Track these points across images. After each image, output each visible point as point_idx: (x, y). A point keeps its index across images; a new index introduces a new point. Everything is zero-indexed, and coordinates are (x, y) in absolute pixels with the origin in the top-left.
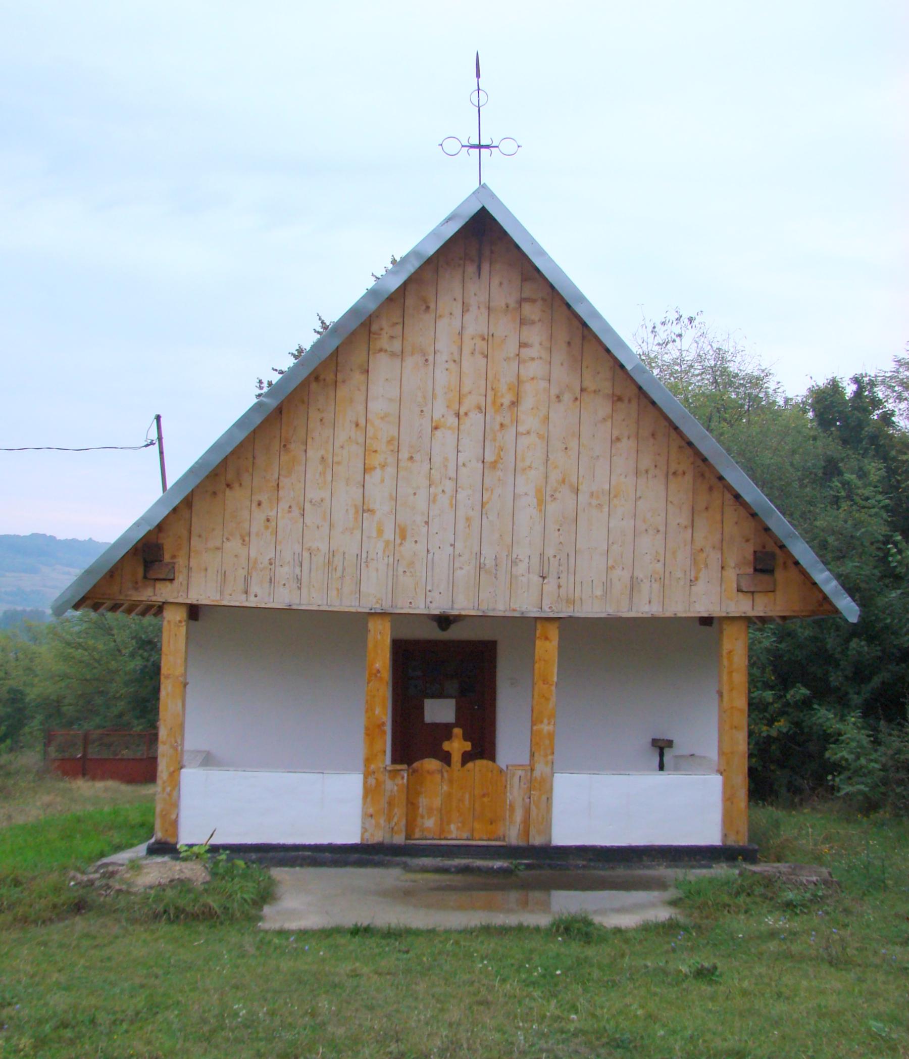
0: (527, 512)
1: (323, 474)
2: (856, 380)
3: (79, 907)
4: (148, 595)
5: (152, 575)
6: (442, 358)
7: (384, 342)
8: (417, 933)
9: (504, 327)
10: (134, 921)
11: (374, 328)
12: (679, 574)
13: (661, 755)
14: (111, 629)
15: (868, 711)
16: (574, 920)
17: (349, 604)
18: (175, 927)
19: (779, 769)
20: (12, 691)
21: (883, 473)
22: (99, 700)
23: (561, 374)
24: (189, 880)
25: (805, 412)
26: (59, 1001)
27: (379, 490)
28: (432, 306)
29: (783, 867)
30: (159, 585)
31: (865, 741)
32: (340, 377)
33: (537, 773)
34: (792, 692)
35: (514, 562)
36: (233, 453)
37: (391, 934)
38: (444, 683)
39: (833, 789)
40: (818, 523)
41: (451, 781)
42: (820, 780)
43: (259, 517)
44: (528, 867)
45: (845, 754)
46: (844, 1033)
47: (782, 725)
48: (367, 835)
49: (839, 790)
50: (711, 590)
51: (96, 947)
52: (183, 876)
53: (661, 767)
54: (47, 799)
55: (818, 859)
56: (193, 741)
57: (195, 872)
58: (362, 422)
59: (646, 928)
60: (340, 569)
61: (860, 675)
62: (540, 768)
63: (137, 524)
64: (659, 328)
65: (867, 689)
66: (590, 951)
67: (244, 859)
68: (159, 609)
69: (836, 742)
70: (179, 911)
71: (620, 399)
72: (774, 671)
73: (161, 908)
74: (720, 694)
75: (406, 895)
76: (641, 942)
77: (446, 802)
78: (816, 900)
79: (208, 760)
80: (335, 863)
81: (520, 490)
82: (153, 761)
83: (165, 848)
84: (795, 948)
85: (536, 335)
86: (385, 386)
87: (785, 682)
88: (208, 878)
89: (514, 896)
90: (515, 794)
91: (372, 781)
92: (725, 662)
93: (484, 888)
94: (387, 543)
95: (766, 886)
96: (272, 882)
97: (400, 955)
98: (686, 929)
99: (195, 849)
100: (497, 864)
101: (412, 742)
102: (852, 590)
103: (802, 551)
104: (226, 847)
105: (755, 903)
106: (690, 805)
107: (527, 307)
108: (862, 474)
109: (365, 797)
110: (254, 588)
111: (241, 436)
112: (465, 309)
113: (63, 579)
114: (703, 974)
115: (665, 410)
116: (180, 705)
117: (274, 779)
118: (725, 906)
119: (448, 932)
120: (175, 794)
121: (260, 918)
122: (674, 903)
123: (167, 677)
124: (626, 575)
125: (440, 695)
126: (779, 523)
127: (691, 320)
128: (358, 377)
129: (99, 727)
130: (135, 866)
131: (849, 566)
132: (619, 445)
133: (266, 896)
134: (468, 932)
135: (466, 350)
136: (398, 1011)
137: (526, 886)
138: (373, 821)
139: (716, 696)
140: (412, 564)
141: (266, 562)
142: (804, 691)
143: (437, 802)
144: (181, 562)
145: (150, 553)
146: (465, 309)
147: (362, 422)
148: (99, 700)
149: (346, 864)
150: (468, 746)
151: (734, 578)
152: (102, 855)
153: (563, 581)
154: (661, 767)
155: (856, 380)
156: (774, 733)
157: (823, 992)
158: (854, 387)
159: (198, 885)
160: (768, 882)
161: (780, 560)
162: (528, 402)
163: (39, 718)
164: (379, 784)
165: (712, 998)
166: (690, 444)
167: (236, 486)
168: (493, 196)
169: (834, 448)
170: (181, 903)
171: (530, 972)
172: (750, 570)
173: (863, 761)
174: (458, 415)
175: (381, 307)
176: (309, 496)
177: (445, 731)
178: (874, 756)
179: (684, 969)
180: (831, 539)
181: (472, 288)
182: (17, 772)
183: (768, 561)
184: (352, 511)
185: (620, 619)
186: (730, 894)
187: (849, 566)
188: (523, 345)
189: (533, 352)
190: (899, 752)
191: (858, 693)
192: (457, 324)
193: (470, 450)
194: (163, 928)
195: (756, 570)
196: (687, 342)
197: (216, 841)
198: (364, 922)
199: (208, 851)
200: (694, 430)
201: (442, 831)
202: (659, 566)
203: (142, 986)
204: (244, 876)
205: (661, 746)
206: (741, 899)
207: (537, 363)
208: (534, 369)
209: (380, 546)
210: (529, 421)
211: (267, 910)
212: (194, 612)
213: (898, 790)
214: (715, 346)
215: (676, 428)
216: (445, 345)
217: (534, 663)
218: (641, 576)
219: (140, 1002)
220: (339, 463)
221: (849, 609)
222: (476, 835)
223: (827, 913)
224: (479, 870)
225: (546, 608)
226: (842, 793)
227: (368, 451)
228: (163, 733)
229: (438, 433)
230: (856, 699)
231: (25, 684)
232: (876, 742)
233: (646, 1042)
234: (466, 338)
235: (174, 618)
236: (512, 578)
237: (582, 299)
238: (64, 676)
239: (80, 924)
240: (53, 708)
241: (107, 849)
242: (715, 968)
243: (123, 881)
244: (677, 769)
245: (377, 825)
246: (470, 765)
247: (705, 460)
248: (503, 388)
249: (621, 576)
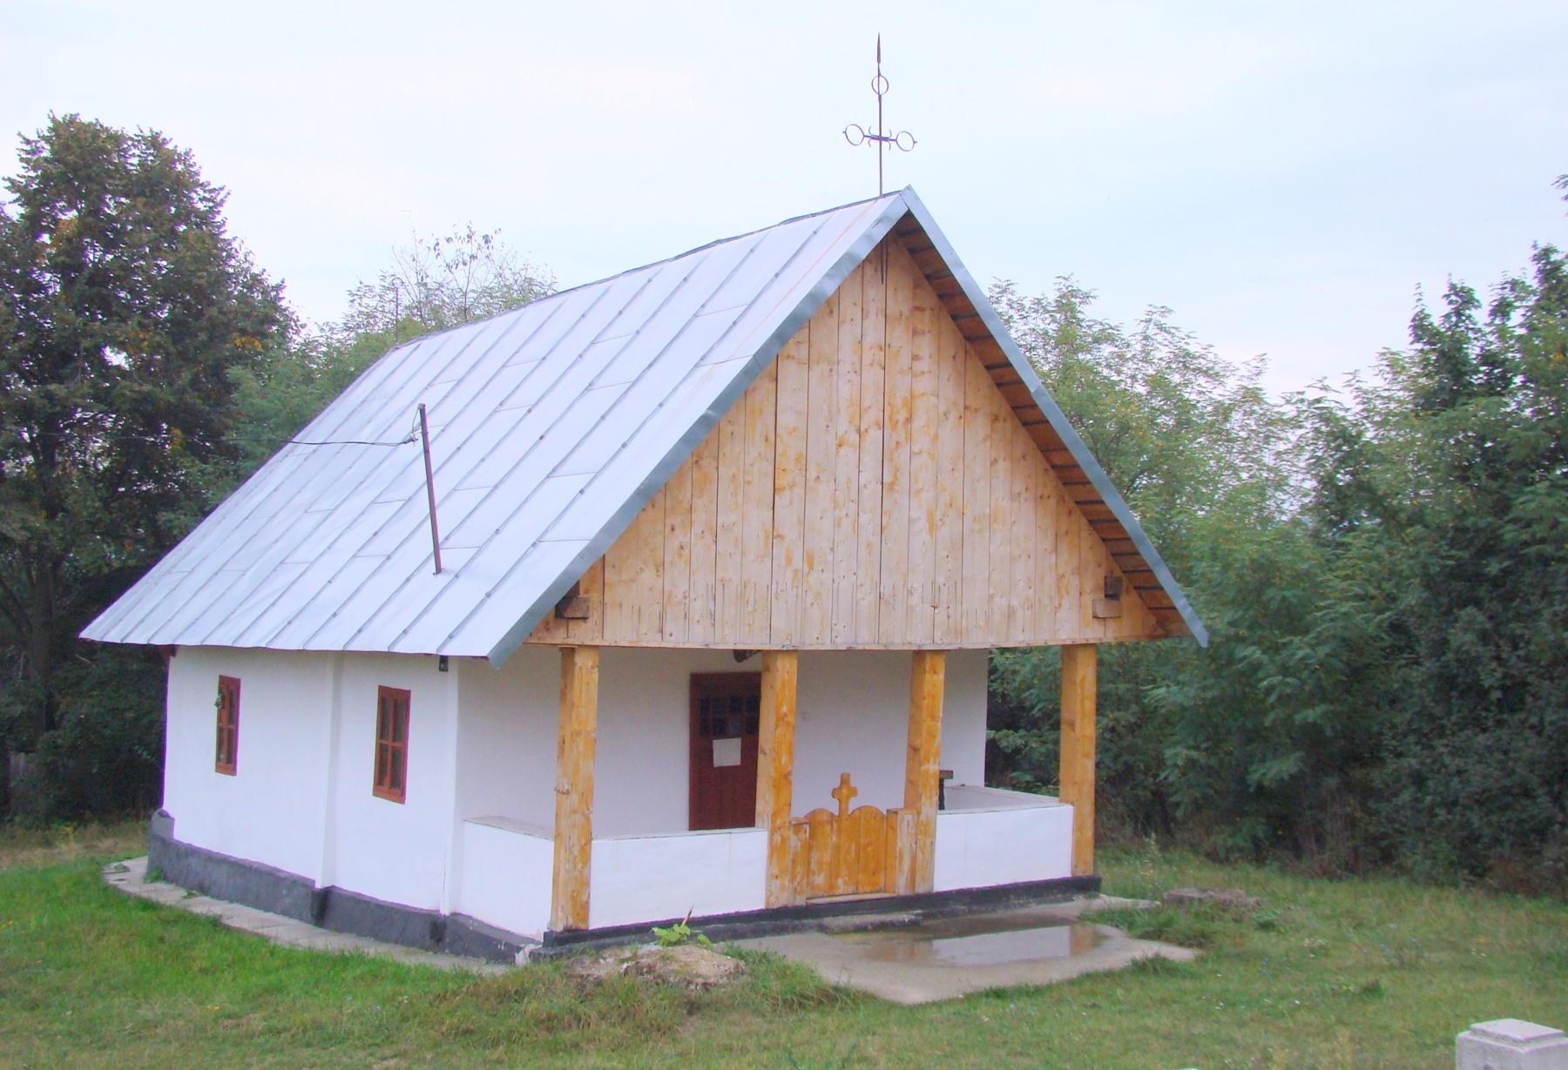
6: (845, 367)
9: (899, 337)
30: (572, 624)
35: (910, 593)
48: (772, 899)
91: (777, 838)
100: (905, 917)
109: (771, 856)
112: (864, 314)
135: (866, 361)
140: (819, 594)
141: (680, 595)
143: (827, 857)
146: (864, 314)
151: (1090, 604)
162: (918, 423)
164: (784, 840)
188: (915, 358)
208: (924, 384)
209: (789, 574)
210: (921, 442)
216: (847, 356)
220: (749, 483)
225: (937, 640)
229: (842, 451)
234: (866, 346)
236: (909, 610)
245: (782, 886)
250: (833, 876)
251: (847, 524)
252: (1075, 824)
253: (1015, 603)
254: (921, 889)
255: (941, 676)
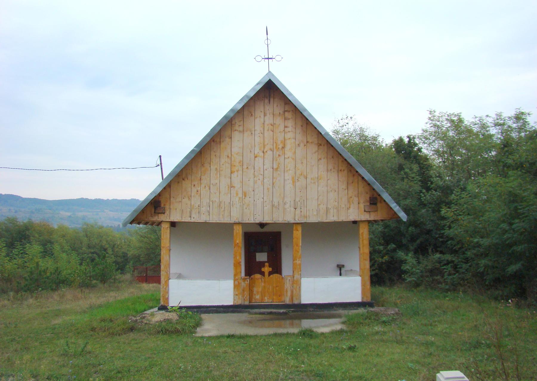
0: (289, 185)
1: (216, 174)
2: (408, 137)
3: (132, 329)
4: (156, 219)
5: (157, 211)
7: (237, 127)
8: (250, 336)
9: (279, 121)
10: (150, 334)
11: (233, 123)
12: (343, 206)
13: (340, 270)
14: (156, 231)
15: (416, 252)
16: (307, 330)
17: (227, 220)
18: (165, 336)
19: (383, 274)
20: (123, 253)
21: (418, 168)
22: (152, 256)
23: (300, 136)
24: (171, 319)
25: (391, 148)
26: (118, 364)
27: (236, 179)
28: (253, 114)
29: (382, 308)
30: (159, 215)
31: (415, 262)
32: (221, 140)
33: (295, 278)
34: (390, 246)
35: (285, 204)
36: (184, 168)
37: (241, 337)
38: (263, 248)
39: (404, 280)
40: (396, 187)
41: (265, 282)
42: (400, 276)
43: (194, 190)
44: (293, 311)
45: (408, 267)
46: (400, 368)
47: (386, 258)
48: (235, 302)
49: (406, 280)
50: (355, 212)
51: (137, 343)
52: (169, 318)
53: (340, 275)
54: (132, 290)
55: (396, 305)
56: (173, 270)
57: (173, 316)
58: (230, 156)
59: (333, 332)
60: (223, 208)
61: (413, 239)
62: (296, 276)
63: (151, 194)
64: (340, 121)
65: (415, 245)
66: (312, 342)
67: (192, 311)
68: (159, 224)
69: (405, 263)
70: (167, 330)
71: (321, 145)
72: (383, 239)
73: (160, 329)
74: (359, 248)
75: (250, 323)
76: (330, 337)
77: (264, 289)
78: (394, 320)
79: (180, 276)
80: (225, 312)
81: (286, 178)
82: (159, 277)
83: (164, 308)
84: (385, 338)
85: (290, 123)
86: (237, 143)
87: (387, 243)
88: (178, 318)
89: (288, 322)
90: (288, 285)
91: (236, 283)
92: (361, 237)
93: (278, 319)
94: (240, 198)
95: (376, 316)
96: (201, 319)
97: (244, 345)
98: (346, 332)
99: (174, 308)
101: (252, 268)
102: (406, 210)
103: (386, 196)
104: (185, 307)
105: (372, 322)
106: (349, 287)
107: (286, 114)
108: (411, 169)
109: (234, 288)
110: (193, 215)
111: (187, 162)
112: (265, 115)
113: (126, 214)
114: (351, 348)
115: (336, 148)
116: (168, 256)
117: (200, 284)
118: (361, 323)
119: (261, 336)
120: (167, 288)
121: (195, 333)
122: (343, 323)
123: (163, 247)
124: (325, 207)
125: (262, 251)
126: (377, 186)
127: (351, 118)
128: (228, 140)
129: (153, 265)
130: (152, 315)
131: (408, 202)
132: (320, 161)
133: (198, 324)
134: (268, 336)
135: (266, 129)
136: (239, 365)
137: (291, 318)
138: (237, 297)
139: (358, 249)
141: (197, 206)
142: (394, 246)
143: (260, 290)
144: (167, 207)
145: (156, 204)
146: (265, 115)
147: (230, 156)
148: (152, 256)
149: (228, 312)
150: (271, 269)
152: (145, 310)
153: (302, 210)
154: (340, 275)
155: (408, 137)
156: (384, 261)
157: (393, 353)
158: (408, 139)
159: (174, 321)
160: (377, 314)
161: (379, 200)
162: (288, 147)
163: (132, 262)
165: (354, 357)
166: (346, 160)
167: (186, 179)
168: (273, 75)
169: (402, 161)
170: (167, 327)
171: (289, 350)
172: (369, 204)
173: (414, 269)
174: (264, 152)
175: (235, 114)
176: (212, 182)
177: (262, 264)
178: (418, 267)
179: (344, 347)
180: (401, 192)
181: (267, 107)
182: (123, 281)
183: (374, 201)
184: (227, 187)
185: (323, 222)
186: (363, 319)
187: (408, 202)
188: (286, 127)
189: (290, 129)
190: (427, 266)
191: (412, 246)
192: (262, 120)
193: (268, 165)
194: (160, 336)
195: (370, 204)
196: (350, 126)
197: (181, 305)
198: (232, 333)
199: (178, 309)
200: (347, 155)
201: (262, 299)
202: (336, 203)
203: (149, 358)
204: (191, 317)
205: (340, 267)
206: (367, 321)
207: (291, 134)
208: (290, 135)
209: (237, 199)
210: (289, 154)
211: (198, 329)
212: (173, 224)
213: (427, 279)
214: (360, 127)
215: (341, 155)
216: (258, 128)
217: (293, 239)
218: (330, 207)
219: (147, 364)
221: (403, 216)
222: (274, 301)
223: (397, 325)
224: (275, 313)
226: (407, 281)
227: (232, 166)
228: (162, 267)
229: (257, 159)
230: (412, 248)
231: (128, 251)
232: (419, 263)
233: (328, 374)
234: (266, 126)
235: (165, 227)
237: (305, 110)
238: (141, 248)
239: (132, 335)
240: (137, 258)
241: (147, 308)
242: (355, 346)
243: (148, 320)
244: (346, 275)
245: (239, 298)
246: (271, 276)
247: (351, 165)
248: (279, 142)
249: (323, 207)
250: (263, 296)
251: (259, 182)
252: (362, 283)
253: (329, 206)
254: (296, 302)
255: (300, 232)
